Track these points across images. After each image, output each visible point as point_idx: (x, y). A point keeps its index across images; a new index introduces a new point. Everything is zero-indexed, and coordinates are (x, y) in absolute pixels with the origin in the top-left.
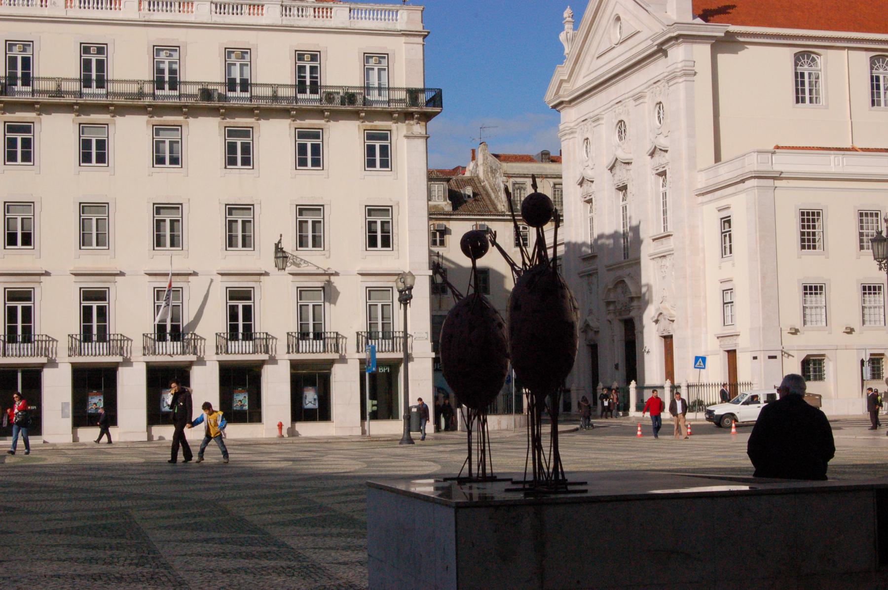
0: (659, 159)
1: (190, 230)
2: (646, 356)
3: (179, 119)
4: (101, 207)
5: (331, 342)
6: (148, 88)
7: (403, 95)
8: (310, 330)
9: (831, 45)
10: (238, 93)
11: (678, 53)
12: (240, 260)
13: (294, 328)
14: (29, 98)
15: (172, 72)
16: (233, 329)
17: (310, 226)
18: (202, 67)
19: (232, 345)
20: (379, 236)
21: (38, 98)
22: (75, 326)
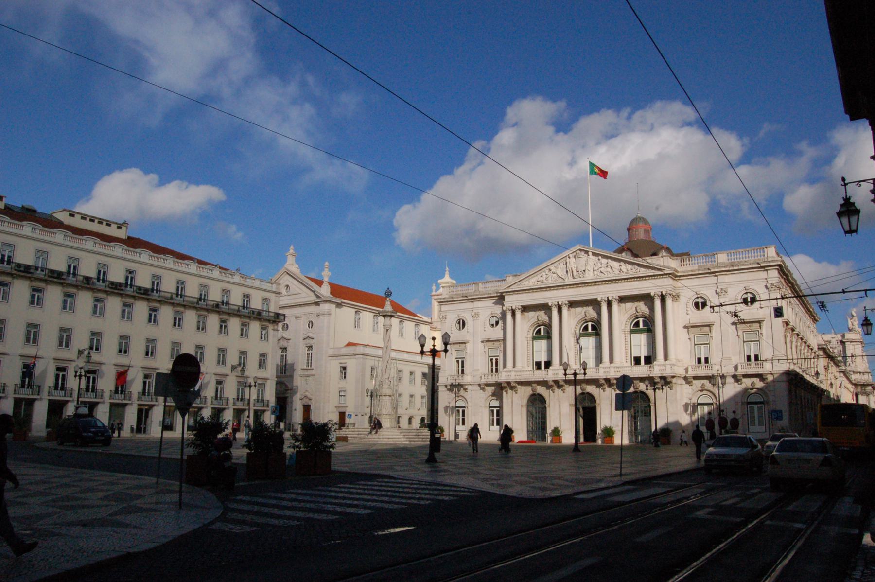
0: (309, 342)
1: (43, 337)
2: (294, 412)
3: (206, 313)
4: (69, 330)
5: (225, 401)
6: (174, 296)
7: (81, 278)
8: (240, 398)
9: (365, 310)
10: (224, 306)
11: (497, 344)
12: (65, 354)
13: (235, 397)
14: (157, 298)
15: (9, 257)
16: (144, 390)
17: (96, 341)
18: (215, 296)
19: (217, 402)
20: (149, 352)
21: (161, 299)
22: (18, 380)
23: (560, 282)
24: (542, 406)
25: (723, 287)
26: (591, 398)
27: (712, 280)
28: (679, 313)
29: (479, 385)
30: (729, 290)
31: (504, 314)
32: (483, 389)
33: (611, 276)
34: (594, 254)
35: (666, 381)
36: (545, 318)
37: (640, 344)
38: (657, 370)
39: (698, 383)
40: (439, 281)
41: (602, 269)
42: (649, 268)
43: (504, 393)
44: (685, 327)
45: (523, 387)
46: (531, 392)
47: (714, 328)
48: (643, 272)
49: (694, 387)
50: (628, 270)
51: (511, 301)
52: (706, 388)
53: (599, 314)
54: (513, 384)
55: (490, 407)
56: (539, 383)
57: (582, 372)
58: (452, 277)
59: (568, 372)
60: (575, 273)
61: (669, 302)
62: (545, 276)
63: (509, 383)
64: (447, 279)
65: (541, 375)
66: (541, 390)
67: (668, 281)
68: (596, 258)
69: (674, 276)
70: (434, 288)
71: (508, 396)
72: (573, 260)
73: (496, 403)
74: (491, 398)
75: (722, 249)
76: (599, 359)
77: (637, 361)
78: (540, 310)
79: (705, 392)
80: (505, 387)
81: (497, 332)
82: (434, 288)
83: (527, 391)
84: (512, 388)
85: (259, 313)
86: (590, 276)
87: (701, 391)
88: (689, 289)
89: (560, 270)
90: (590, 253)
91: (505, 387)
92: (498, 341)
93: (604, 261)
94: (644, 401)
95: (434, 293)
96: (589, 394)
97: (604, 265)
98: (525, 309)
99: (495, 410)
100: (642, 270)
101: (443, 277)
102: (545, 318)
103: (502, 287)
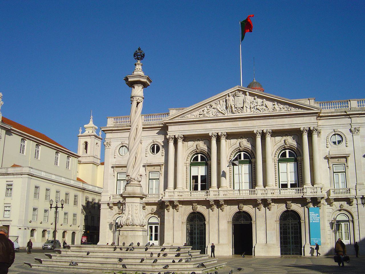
23: (220, 116)
24: (202, 223)
25: (357, 127)
26: (247, 216)
27: (347, 121)
28: (322, 146)
29: (108, 204)
30: (361, 129)
31: (166, 142)
32: (111, 208)
33: (266, 113)
34: (251, 94)
35: (315, 201)
36: (204, 148)
37: (288, 172)
38: (309, 192)
39: (337, 204)
40: (85, 126)
41: (258, 107)
42: (299, 107)
43: (166, 211)
44: (326, 158)
45: (276, 205)
46: (192, 211)
47: (349, 159)
48: (294, 111)
49: (334, 207)
50: (280, 109)
51: (173, 131)
52: (344, 208)
53: (254, 145)
54: (111, 205)
55: (149, 223)
56: (199, 202)
57: (61, 206)
58: (94, 123)
59: (52, 206)
60: (234, 109)
61: (315, 136)
62: (206, 110)
63: (172, 203)
64: (91, 124)
65: (200, 195)
66: (201, 209)
67: (313, 119)
68: (252, 99)
69: (318, 116)
70: (81, 131)
71: (169, 214)
72: (231, 98)
73: (155, 220)
74: (150, 215)
75: (354, 98)
76: (253, 183)
77: (284, 186)
78: (198, 140)
79: (342, 212)
80: (167, 206)
81: (159, 158)
82: (81, 131)
83: (186, 211)
84: (175, 207)
85: (37, 270)
86: (248, 112)
87: (340, 210)
88: (326, 128)
89: (221, 107)
90: (247, 93)
91: (167, 206)
92: (159, 165)
93: (259, 101)
94: (295, 219)
95: (80, 134)
96: (245, 212)
97: (260, 104)
98: (186, 138)
99: (154, 226)
100: (293, 109)
101: (88, 123)
102: (204, 148)
103: (166, 119)
